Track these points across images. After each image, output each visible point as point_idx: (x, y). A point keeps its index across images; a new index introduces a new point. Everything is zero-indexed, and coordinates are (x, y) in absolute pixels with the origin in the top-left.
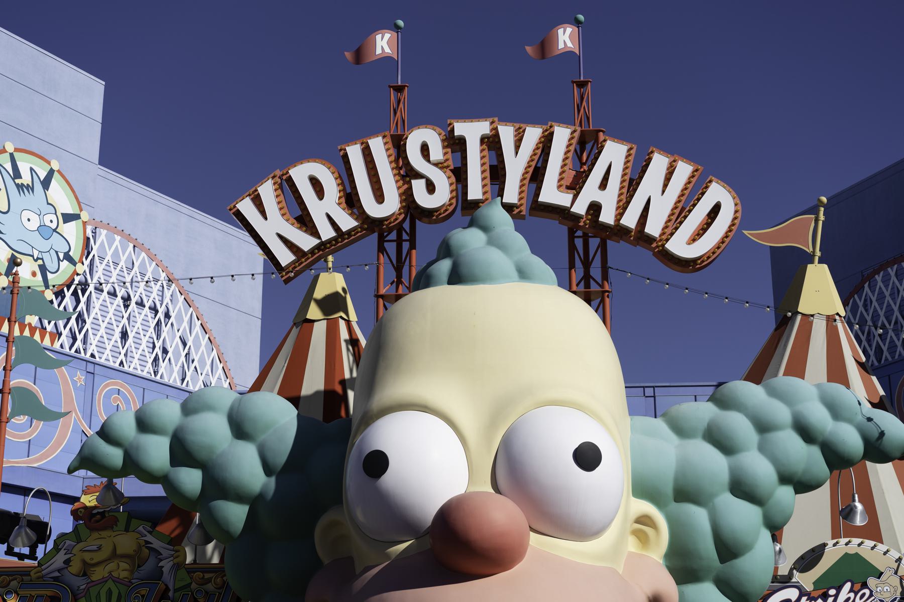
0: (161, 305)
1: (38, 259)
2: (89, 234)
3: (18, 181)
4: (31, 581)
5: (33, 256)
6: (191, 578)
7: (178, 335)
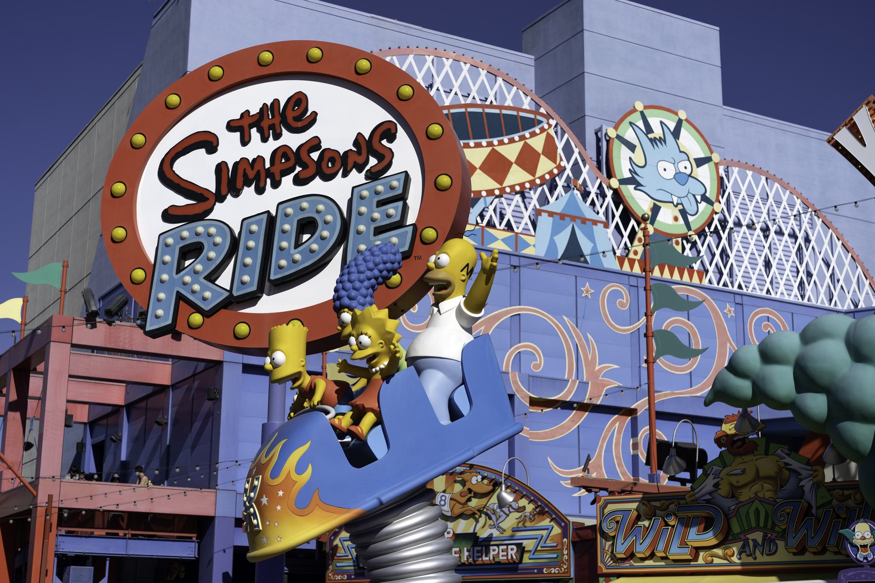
0: (800, 230)
1: (678, 204)
2: (722, 172)
3: (651, 136)
4: (687, 504)
5: (672, 203)
6: (831, 495)
7: (820, 257)
